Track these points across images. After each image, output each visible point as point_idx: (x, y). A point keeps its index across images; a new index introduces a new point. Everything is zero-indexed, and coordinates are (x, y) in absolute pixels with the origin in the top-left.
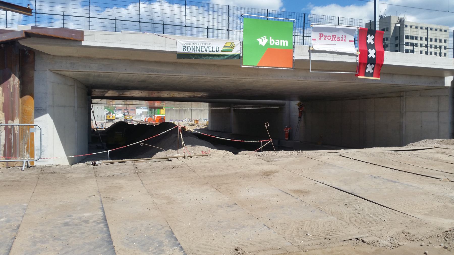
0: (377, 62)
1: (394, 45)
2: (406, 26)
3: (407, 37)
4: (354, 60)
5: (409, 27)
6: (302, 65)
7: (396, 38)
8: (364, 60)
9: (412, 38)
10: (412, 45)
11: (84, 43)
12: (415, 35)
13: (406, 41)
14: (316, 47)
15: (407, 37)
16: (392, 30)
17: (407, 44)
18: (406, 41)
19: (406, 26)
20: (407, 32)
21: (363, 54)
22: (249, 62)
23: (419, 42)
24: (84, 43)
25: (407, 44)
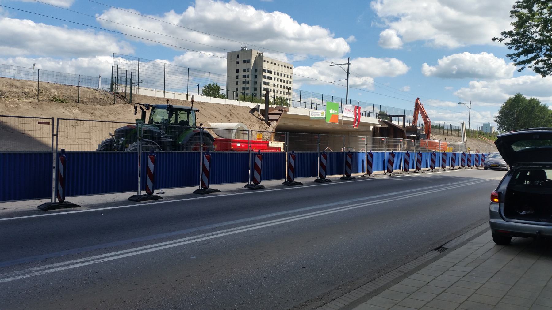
0: (358, 121)
1: (254, 77)
2: (265, 61)
3: (265, 71)
4: (353, 120)
5: (266, 62)
6: (341, 122)
7: (256, 71)
8: (356, 120)
9: (268, 72)
10: (268, 78)
11: (288, 113)
12: (270, 70)
13: (264, 74)
14: (344, 115)
15: (265, 71)
16: (253, 63)
17: (265, 77)
18: (264, 74)
19: (265, 61)
20: (266, 66)
21: (355, 118)
22: (328, 120)
23: (272, 75)
24: (288, 113)
25: (265, 77)
